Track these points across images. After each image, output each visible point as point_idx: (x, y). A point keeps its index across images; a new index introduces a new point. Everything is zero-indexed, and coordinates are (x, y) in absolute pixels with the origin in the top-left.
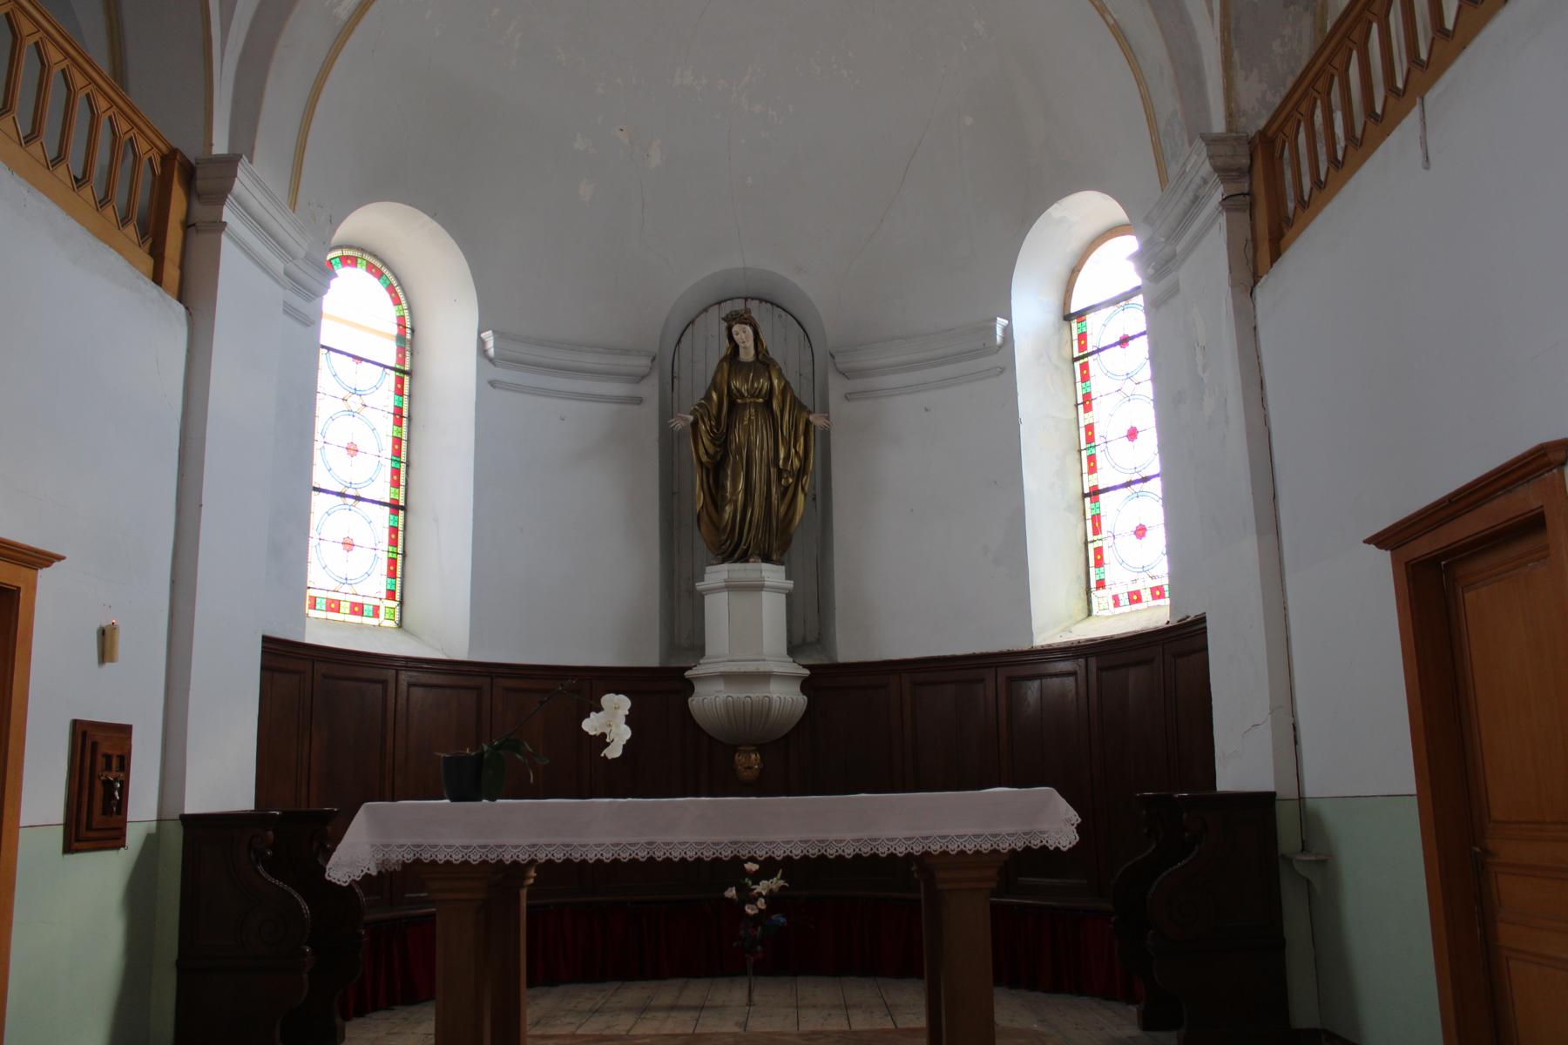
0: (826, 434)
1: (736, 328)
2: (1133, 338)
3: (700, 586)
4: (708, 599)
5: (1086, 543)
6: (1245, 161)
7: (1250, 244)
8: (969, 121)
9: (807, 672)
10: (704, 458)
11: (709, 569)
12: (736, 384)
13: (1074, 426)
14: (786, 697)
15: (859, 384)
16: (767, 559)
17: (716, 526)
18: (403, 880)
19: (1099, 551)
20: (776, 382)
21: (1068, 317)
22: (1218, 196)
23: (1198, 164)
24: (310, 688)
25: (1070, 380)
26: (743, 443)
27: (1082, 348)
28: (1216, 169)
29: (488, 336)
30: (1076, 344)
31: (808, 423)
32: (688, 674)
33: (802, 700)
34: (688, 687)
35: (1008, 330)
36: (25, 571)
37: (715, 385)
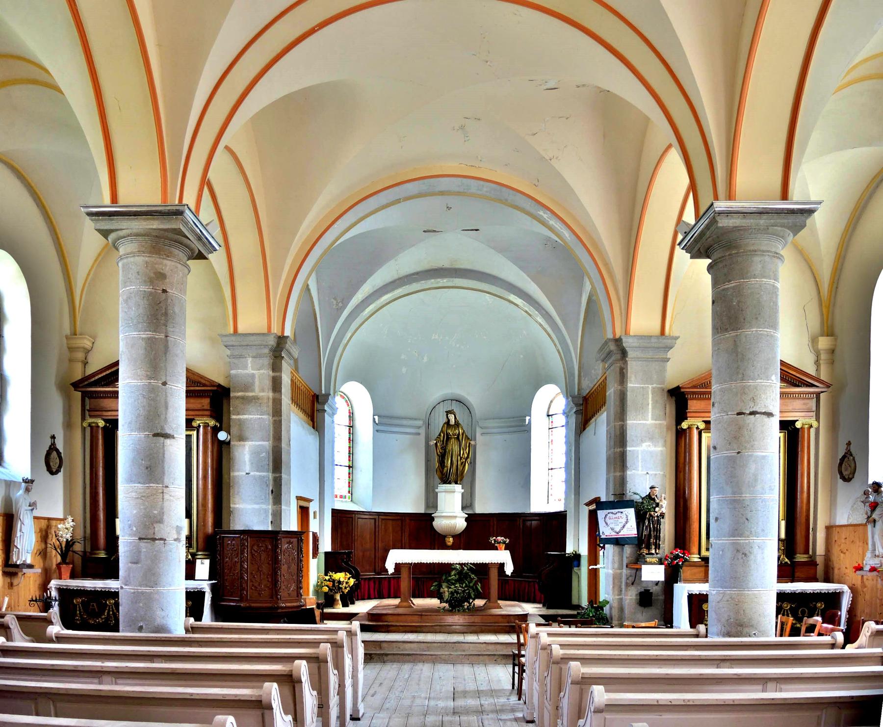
14: (461, 524)
16: (456, 483)
17: (442, 472)
18: (398, 566)
29: (376, 417)
33: (465, 524)
34: (433, 519)
35: (530, 420)
37: (442, 431)
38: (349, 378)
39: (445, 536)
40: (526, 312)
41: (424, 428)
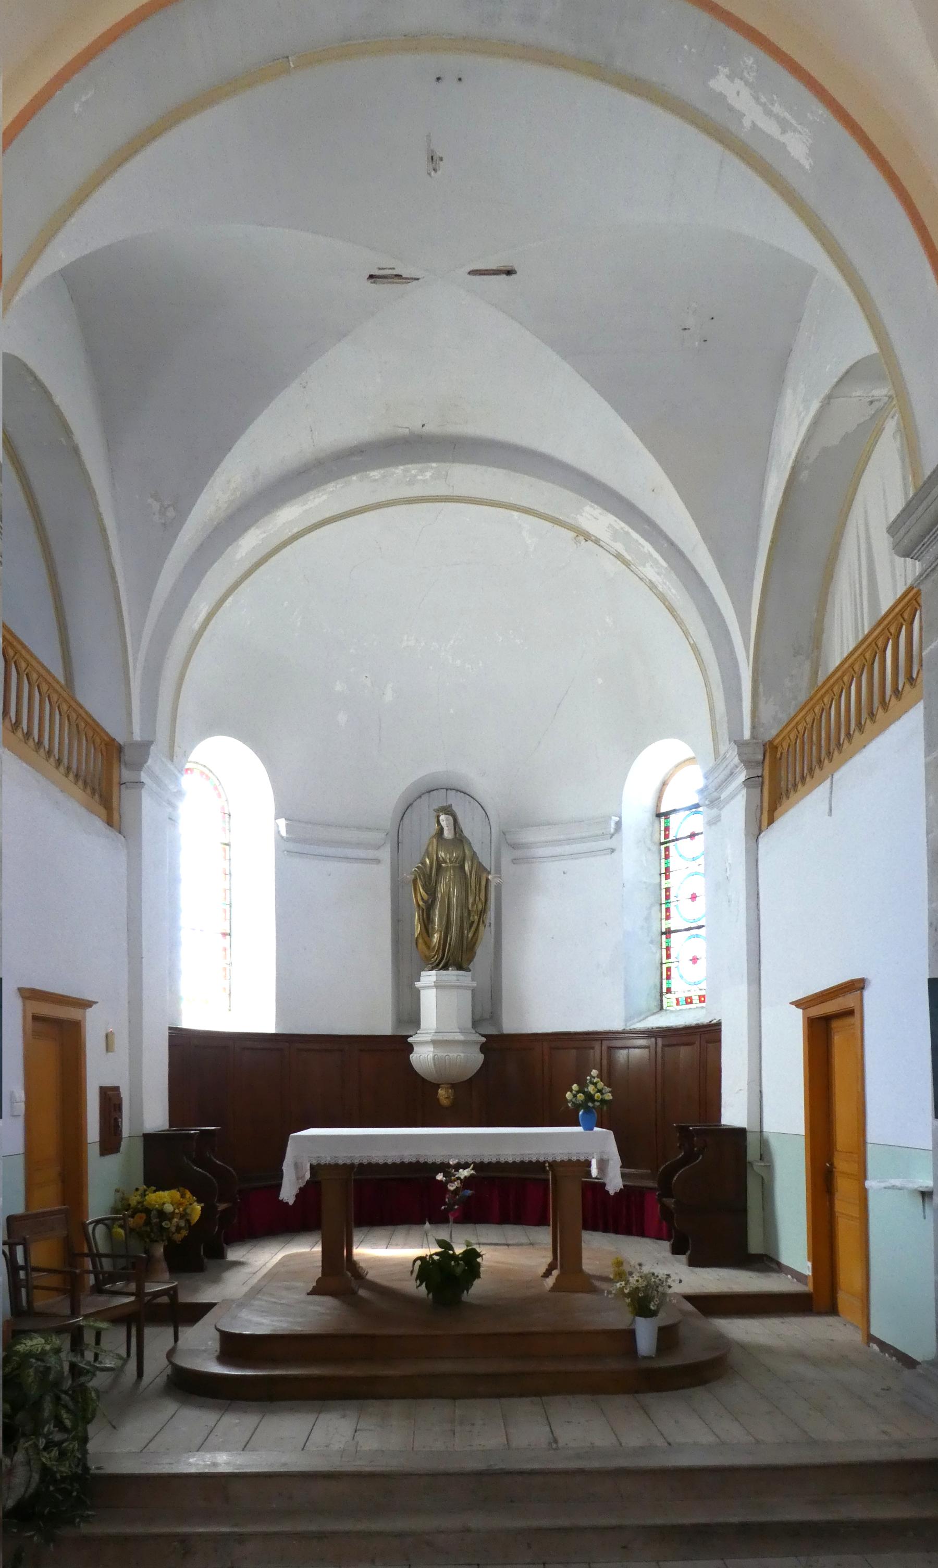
0: (499, 887)
1: (442, 817)
2: (698, 834)
3: (417, 984)
4: (422, 992)
5: (662, 964)
6: (760, 757)
7: (759, 811)
8: (600, 681)
9: (484, 1039)
10: (421, 903)
11: (423, 973)
12: (442, 854)
13: (658, 888)
15: (518, 853)
19: (669, 969)
20: (467, 852)
21: (659, 815)
22: (742, 777)
23: (733, 757)
24: (201, 1061)
25: (657, 858)
26: (451, 899)
27: (666, 836)
28: (742, 761)
29: (282, 823)
30: (663, 833)
31: (487, 880)
32: (410, 1040)
33: (481, 1057)
34: (410, 1048)
36: (80, 1011)
37: (427, 853)
38: (216, 724)
39: (438, 1086)
40: (618, 556)
41: (388, 848)
